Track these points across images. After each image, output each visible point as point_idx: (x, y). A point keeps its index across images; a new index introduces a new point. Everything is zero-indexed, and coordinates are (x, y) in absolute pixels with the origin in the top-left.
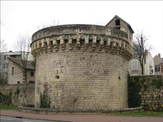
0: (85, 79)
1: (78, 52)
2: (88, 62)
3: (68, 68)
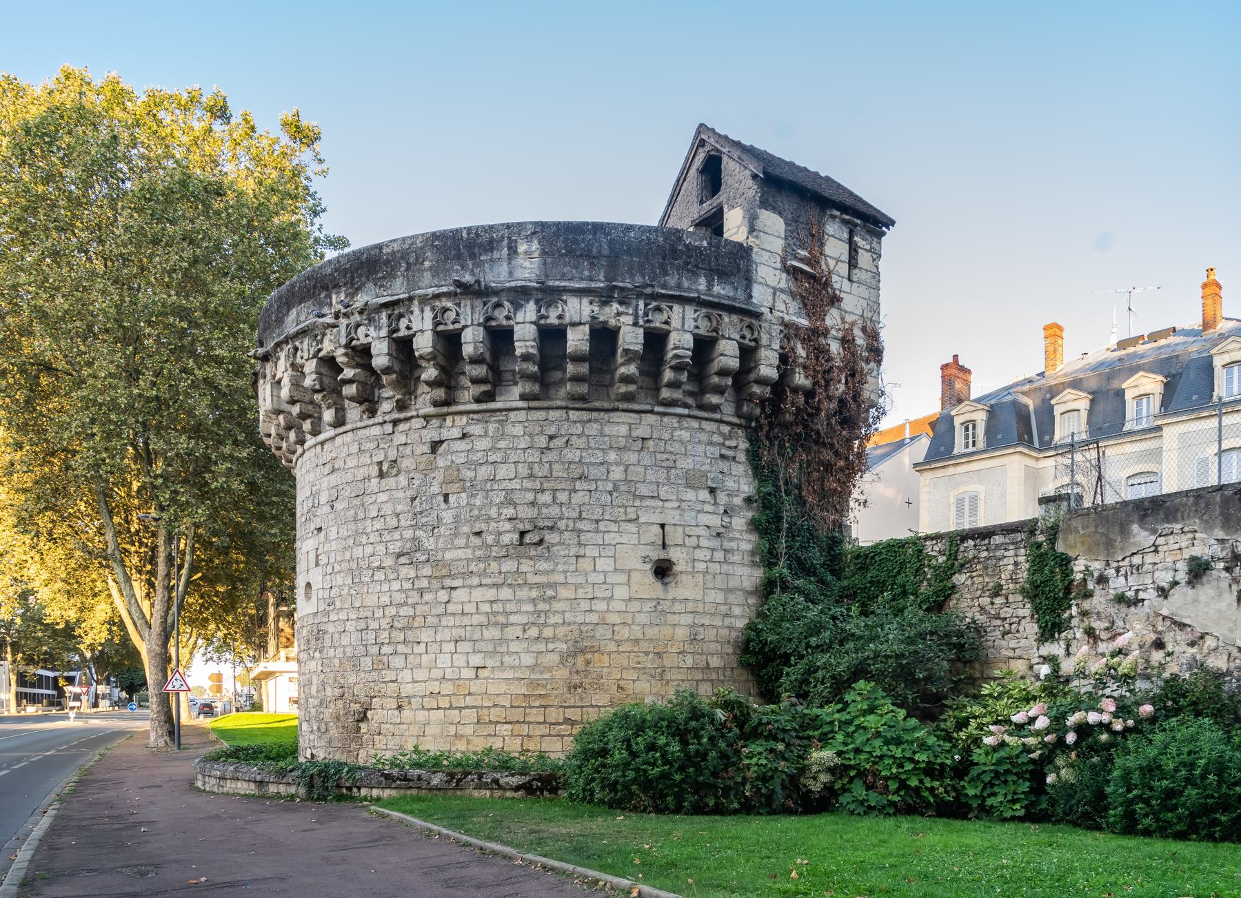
1: (367, 432)
2: (417, 482)
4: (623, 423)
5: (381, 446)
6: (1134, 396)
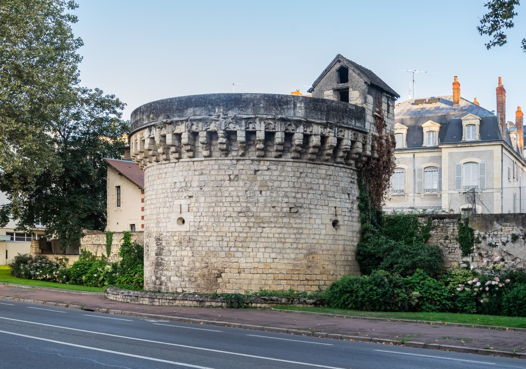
0: (241, 226)
1: (223, 162)
2: (248, 185)
3: (202, 199)
4: (324, 169)
5: (230, 168)
6: (427, 131)
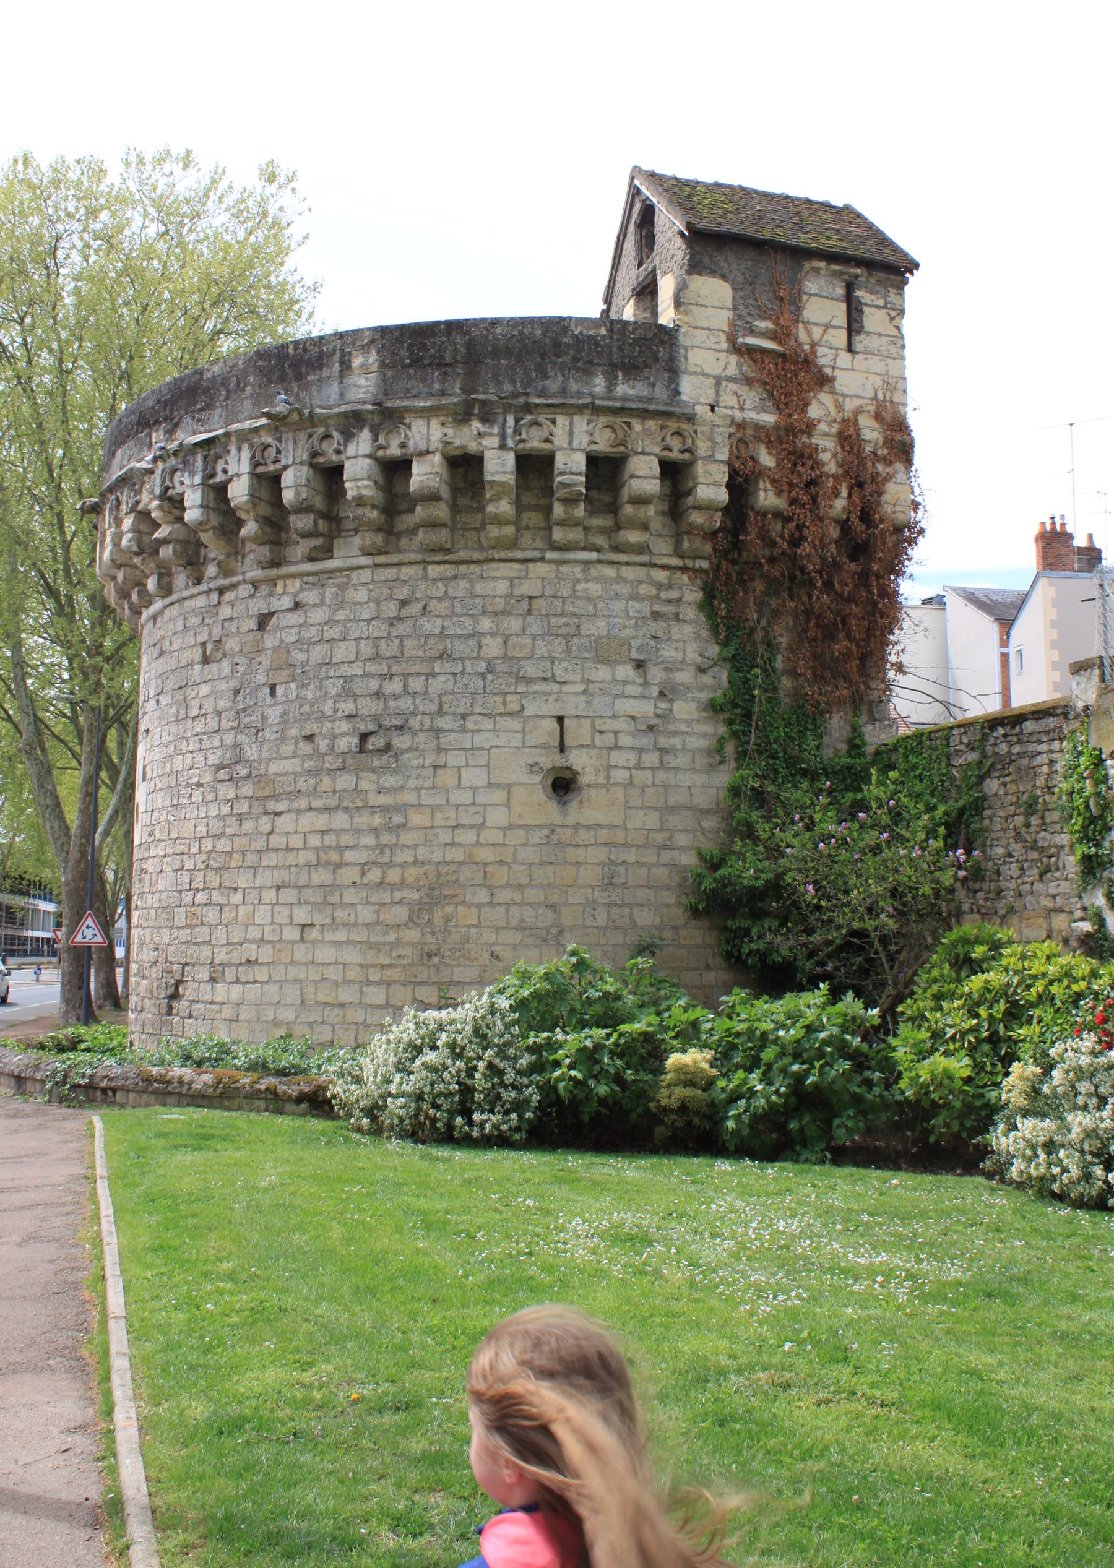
2: (241, 669)
